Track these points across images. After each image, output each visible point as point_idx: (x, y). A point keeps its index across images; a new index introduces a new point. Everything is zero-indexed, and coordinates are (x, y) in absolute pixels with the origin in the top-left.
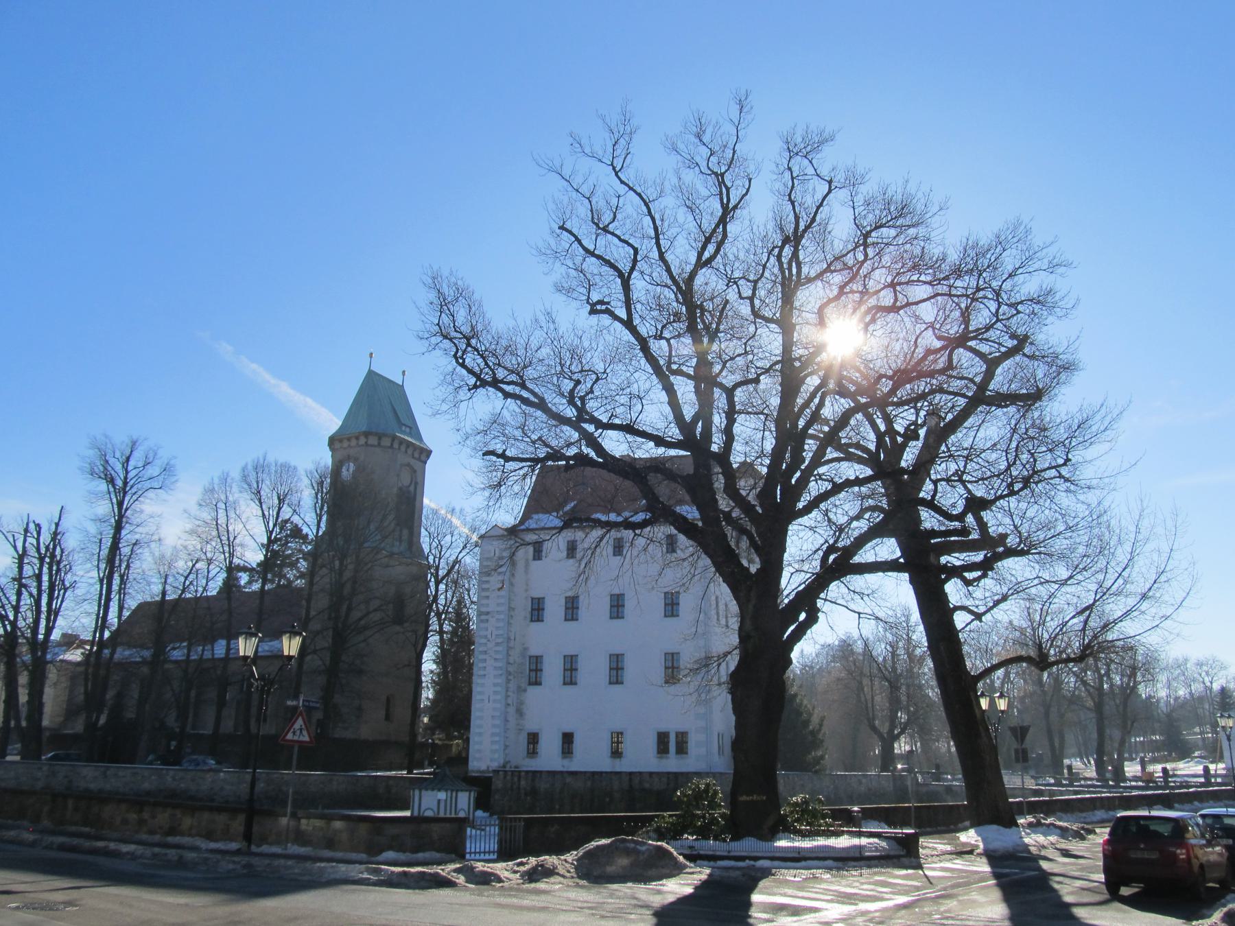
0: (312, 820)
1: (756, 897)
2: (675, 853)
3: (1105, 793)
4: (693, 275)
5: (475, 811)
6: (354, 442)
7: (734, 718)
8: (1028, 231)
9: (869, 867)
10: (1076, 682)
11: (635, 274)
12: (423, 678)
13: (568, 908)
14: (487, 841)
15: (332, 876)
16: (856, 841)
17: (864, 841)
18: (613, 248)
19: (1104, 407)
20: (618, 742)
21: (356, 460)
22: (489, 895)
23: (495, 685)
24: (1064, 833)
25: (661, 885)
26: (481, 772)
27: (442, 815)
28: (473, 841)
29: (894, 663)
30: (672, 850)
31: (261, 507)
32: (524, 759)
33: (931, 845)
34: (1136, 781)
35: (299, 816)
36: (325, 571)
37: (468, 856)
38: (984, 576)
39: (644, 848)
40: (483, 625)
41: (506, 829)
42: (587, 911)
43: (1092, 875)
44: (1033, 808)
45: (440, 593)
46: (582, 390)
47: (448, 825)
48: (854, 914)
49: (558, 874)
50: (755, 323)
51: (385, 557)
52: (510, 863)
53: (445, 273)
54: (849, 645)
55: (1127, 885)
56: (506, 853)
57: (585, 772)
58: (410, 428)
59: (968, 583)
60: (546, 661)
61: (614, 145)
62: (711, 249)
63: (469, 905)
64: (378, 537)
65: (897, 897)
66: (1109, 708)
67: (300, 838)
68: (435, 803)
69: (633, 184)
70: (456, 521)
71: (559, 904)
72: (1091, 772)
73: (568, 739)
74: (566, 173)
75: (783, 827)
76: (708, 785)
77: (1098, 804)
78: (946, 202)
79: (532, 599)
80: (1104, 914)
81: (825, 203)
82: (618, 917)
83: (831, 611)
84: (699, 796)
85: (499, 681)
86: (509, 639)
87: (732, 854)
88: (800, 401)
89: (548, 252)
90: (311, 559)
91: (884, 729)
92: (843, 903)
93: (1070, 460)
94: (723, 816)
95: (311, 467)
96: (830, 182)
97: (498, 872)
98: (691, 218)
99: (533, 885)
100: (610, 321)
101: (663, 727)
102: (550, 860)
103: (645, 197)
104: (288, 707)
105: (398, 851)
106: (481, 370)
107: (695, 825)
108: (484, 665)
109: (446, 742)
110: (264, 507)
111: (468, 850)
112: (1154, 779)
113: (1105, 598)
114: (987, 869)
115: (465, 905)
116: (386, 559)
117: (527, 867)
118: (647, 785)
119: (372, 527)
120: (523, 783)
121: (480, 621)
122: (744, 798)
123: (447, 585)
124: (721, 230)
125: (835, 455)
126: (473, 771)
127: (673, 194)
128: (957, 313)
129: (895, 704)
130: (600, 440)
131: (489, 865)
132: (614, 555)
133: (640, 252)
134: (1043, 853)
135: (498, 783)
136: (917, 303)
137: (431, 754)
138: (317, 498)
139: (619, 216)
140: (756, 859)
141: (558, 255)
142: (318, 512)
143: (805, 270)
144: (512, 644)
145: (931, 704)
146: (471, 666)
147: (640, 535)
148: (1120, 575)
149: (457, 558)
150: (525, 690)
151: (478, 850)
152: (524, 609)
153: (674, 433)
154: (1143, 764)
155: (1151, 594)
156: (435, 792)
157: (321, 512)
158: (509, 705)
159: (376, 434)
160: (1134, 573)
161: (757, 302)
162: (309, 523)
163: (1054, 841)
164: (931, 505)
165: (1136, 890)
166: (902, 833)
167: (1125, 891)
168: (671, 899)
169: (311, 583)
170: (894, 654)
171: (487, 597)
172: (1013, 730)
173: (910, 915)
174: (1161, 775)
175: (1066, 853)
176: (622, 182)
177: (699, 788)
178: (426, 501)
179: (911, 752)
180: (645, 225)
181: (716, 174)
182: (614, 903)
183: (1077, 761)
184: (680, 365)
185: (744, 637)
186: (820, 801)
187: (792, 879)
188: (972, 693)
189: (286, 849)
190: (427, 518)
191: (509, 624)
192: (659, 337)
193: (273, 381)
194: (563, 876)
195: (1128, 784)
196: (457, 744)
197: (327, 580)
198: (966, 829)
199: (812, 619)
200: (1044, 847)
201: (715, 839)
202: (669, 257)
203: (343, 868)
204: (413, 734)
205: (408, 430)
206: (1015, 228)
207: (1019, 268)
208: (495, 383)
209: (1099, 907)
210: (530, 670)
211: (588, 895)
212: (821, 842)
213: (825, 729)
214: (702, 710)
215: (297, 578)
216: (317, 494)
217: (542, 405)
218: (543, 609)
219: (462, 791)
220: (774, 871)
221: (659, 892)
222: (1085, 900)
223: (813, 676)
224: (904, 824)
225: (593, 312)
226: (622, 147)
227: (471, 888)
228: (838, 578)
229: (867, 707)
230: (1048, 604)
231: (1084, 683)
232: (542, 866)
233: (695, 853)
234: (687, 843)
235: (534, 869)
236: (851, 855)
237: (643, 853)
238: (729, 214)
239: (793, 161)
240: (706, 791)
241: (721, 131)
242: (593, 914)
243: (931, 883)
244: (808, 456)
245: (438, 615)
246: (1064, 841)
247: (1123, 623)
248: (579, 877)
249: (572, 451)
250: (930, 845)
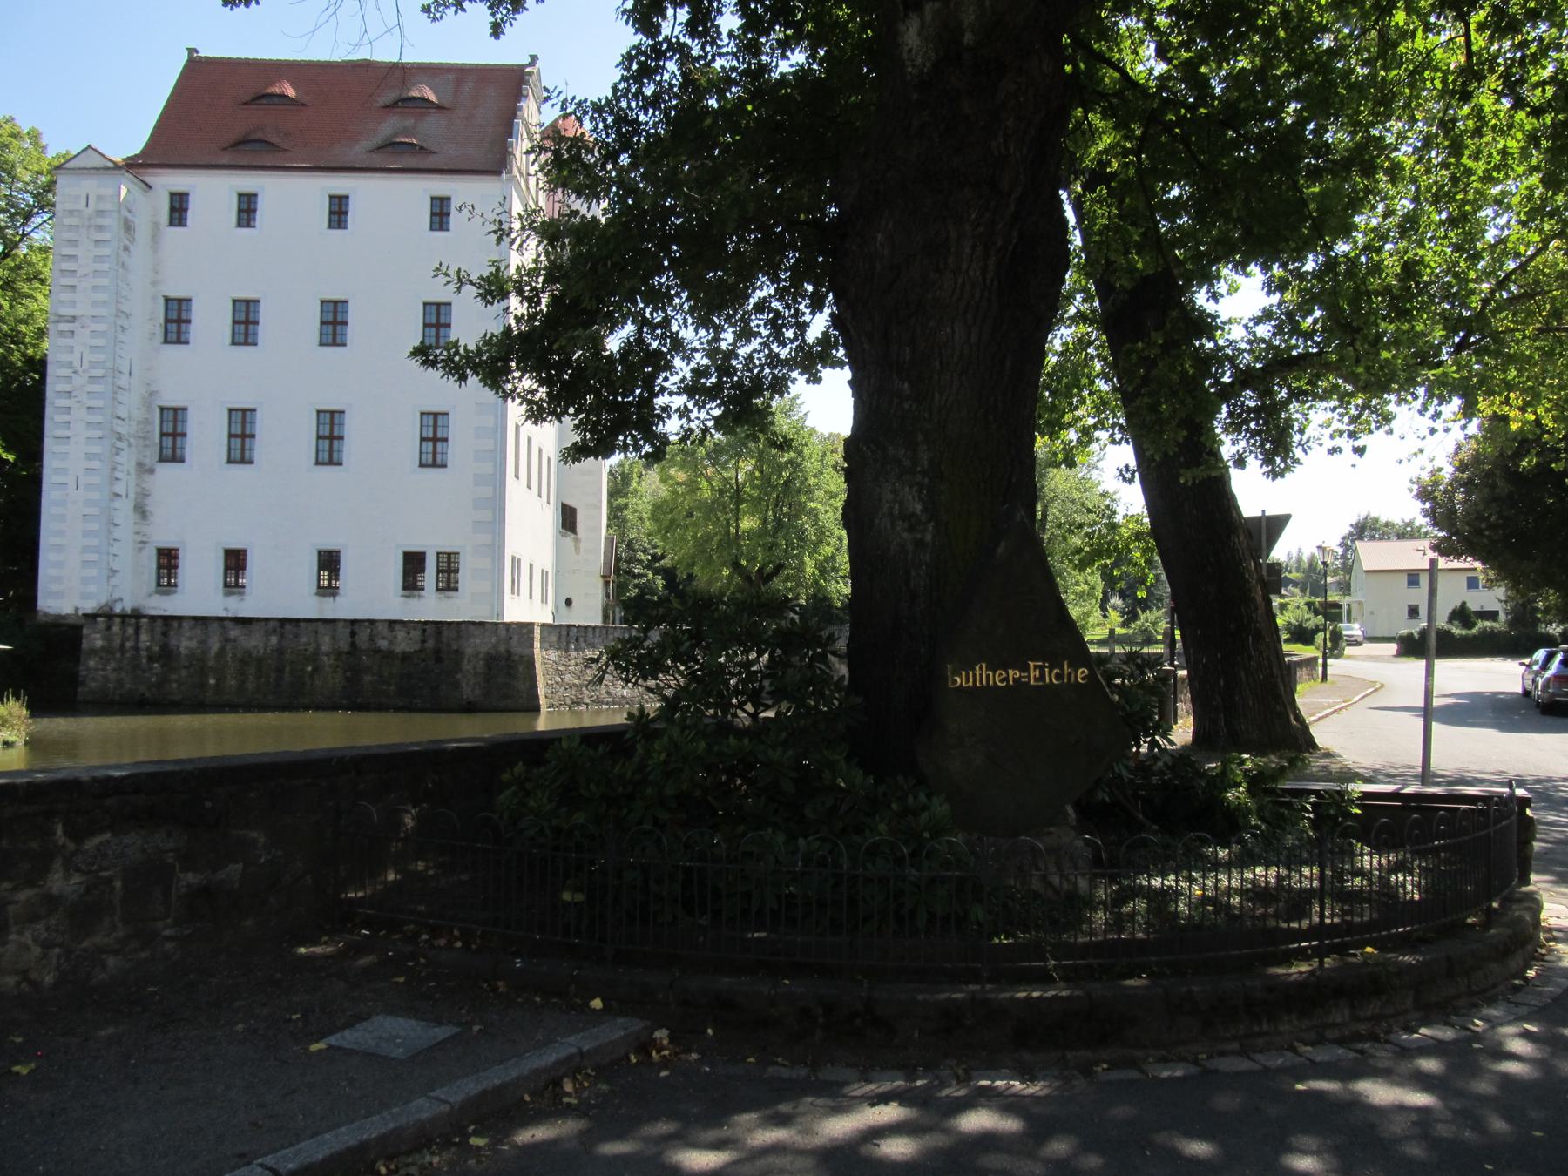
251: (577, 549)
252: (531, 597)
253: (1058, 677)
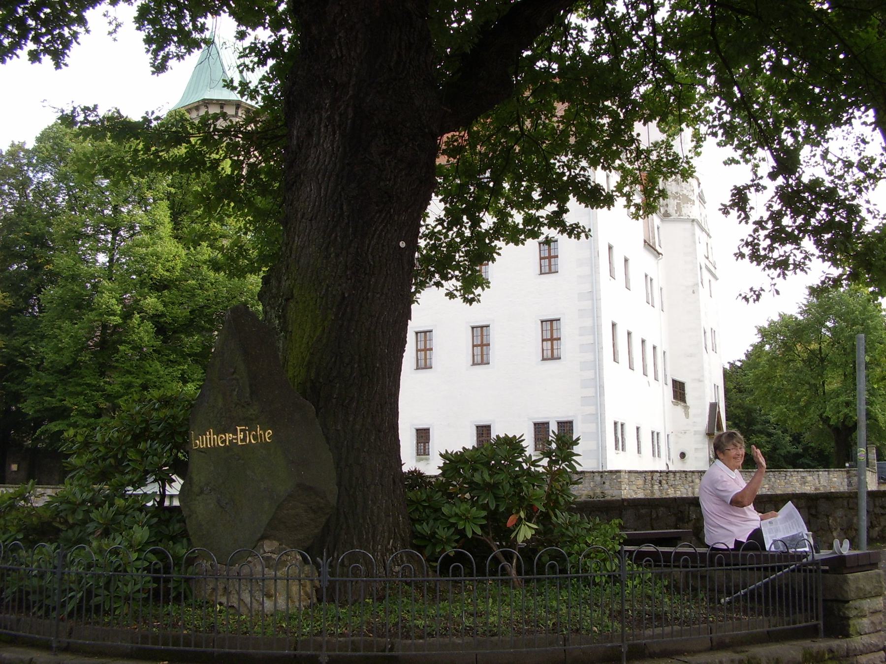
251: (687, 415)
252: (639, 451)
253: (255, 438)
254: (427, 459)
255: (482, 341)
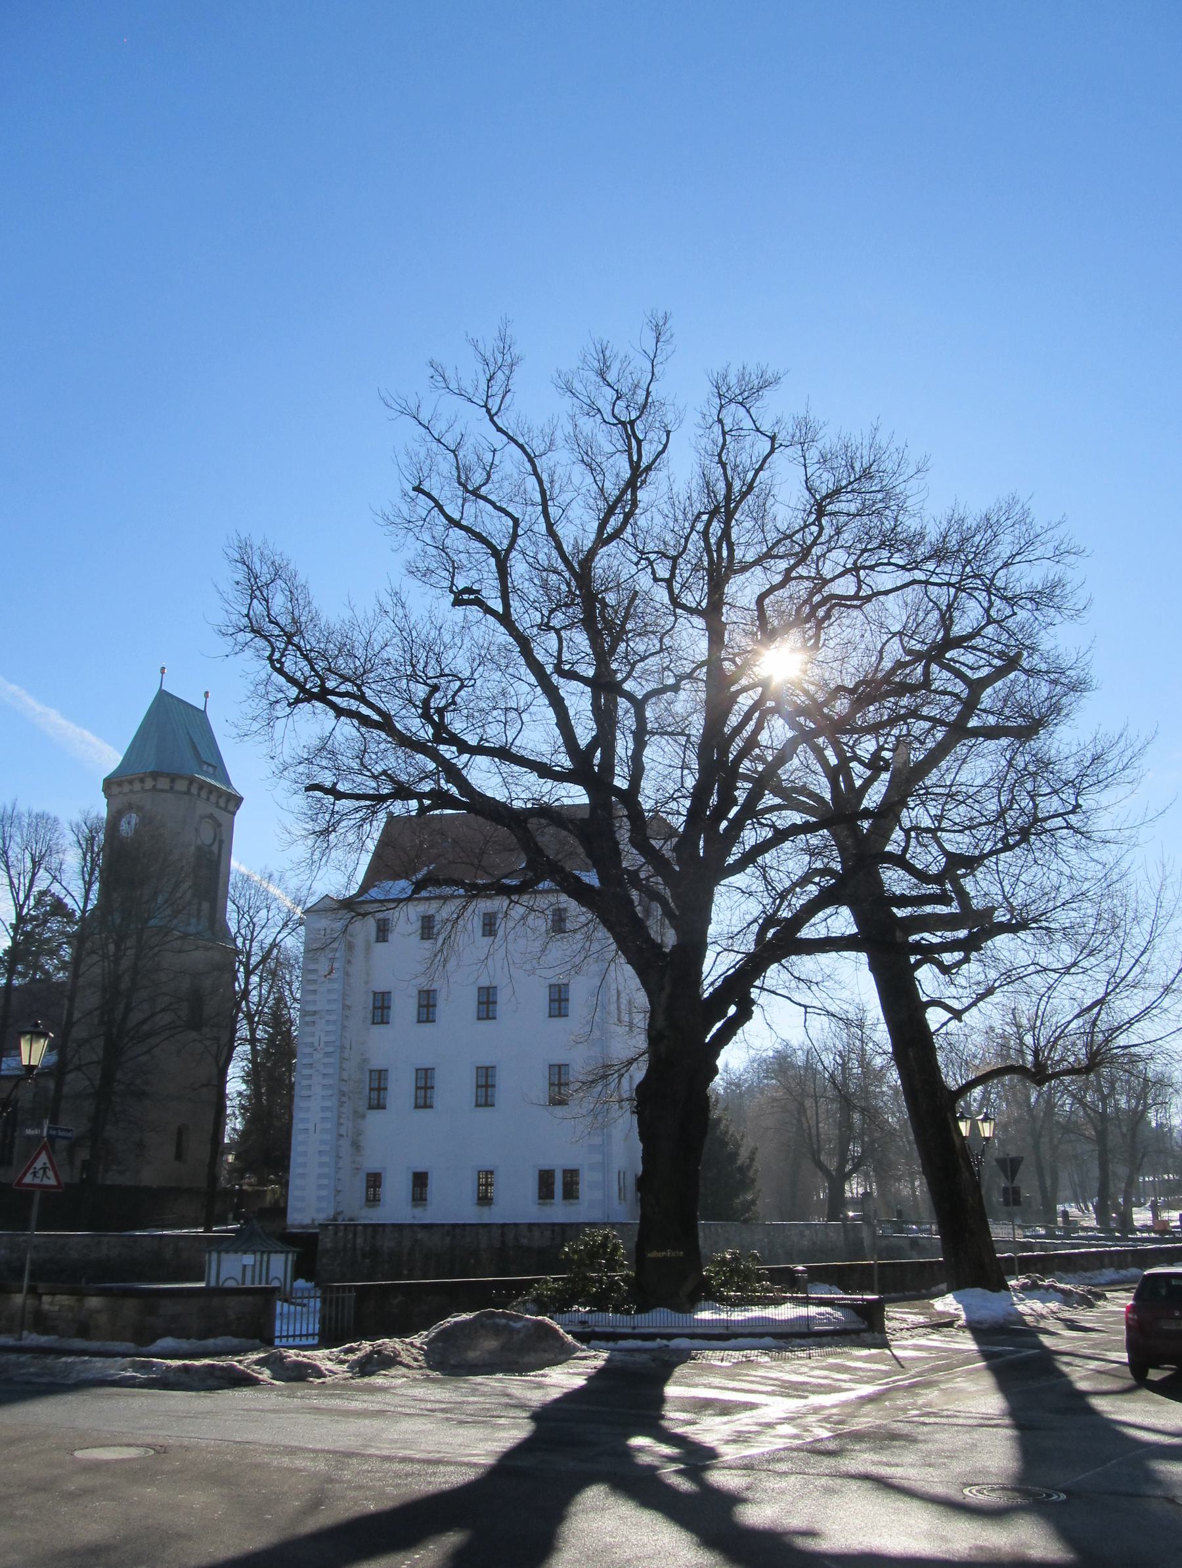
0: (58, 1298)
1: (671, 1390)
2: (561, 1331)
3: (1110, 1246)
4: (592, 553)
5: (295, 1278)
6: (137, 786)
7: (641, 1146)
8: (1026, 513)
9: (820, 1346)
10: (1072, 1105)
11: (513, 554)
12: (228, 1103)
13: (412, 1411)
14: (305, 1322)
15: (83, 1376)
16: (802, 1311)
17: (813, 1311)
18: (486, 519)
19: (1123, 739)
20: (487, 1185)
21: (140, 809)
22: (305, 1396)
23: (324, 1109)
24: (1067, 1298)
25: (542, 1376)
26: (303, 1227)
27: (248, 1285)
28: (285, 1321)
29: (845, 1078)
30: (557, 1327)
31: (8, 872)
32: (361, 1208)
33: (898, 1316)
34: (1149, 1232)
35: (41, 1291)
36: (96, 958)
37: (277, 1342)
38: (966, 960)
39: (519, 1325)
40: (307, 1029)
41: (331, 1303)
42: (440, 1415)
43: (1108, 1353)
44: (1025, 1265)
45: (251, 987)
46: (438, 701)
47: (250, 1298)
48: (804, 1410)
49: (401, 1363)
50: (675, 615)
51: (176, 939)
52: (335, 1350)
53: (257, 542)
54: (785, 1057)
55: (1156, 1366)
56: (329, 1337)
57: (443, 1225)
58: (215, 767)
59: (945, 970)
60: (392, 1076)
61: (489, 381)
62: (614, 522)
63: (274, 1411)
64: (168, 912)
65: (858, 1386)
66: (1114, 1138)
67: (41, 1322)
68: (240, 1269)
69: (513, 431)
70: (274, 890)
71: (400, 1406)
72: (1091, 1221)
73: (420, 1180)
74: (424, 417)
75: (707, 1294)
76: (606, 1237)
77: (1106, 1261)
78: (925, 463)
79: (375, 994)
80: (1132, 1406)
81: (766, 465)
82: (483, 1422)
83: (769, 1005)
84: (594, 1252)
85: (328, 1104)
86: (343, 1047)
87: (637, 1331)
88: (734, 720)
89: (398, 521)
90: (75, 942)
91: (832, 1165)
92: (789, 1396)
93: (1080, 806)
94: (626, 1279)
95: (77, 818)
96: (773, 439)
97: (318, 1363)
98: (590, 479)
99: (366, 1380)
100: (481, 615)
101: (546, 1163)
102: (391, 1344)
103: (529, 450)
104: (29, 1137)
105: (179, 1337)
106: (306, 679)
107: (589, 1292)
108: (309, 1082)
109: (256, 1188)
110: (13, 872)
111: (277, 1334)
112: (1169, 1229)
113: (1117, 990)
114: (972, 1346)
115: (268, 1411)
116: (179, 942)
117: (359, 1354)
118: (525, 1241)
119: (160, 900)
120: (359, 1241)
121: (304, 1024)
122: (654, 1254)
123: (261, 977)
124: (629, 497)
125: (778, 801)
126: (293, 1226)
127: (567, 446)
128: (935, 615)
129: (846, 1133)
130: (464, 772)
131: (306, 1353)
132: (484, 935)
133: (522, 524)
134: (1042, 1325)
135: (326, 1242)
136: (887, 593)
137: (238, 1205)
138: (85, 859)
139: (494, 477)
140: (670, 1337)
141: (411, 526)
142: (87, 878)
143: (738, 553)
144: (346, 1055)
145: (892, 1133)
146: (291, 1086)
147: (517, 903)
148: (1137, 961)
149: (275, 940)
150: (363, 1116)
151: (298, 1333)
152: (362, 1004)
153: (564, 761)
154: (1155, 1209)
155: (1174, 987)
156: (240, 1254)
157: (90, 879)
158: (341, 1136)
159: (168, 775)
160: (1154, 958)
161: (677, 587)
162: (74, 894)
163: (1055, 1309)
164: (900, 861)
165: (1167, 1373)
166: (863, 1300)
167: (1154, 1375)
168: (555, 1394)
169: (76, 975)
170: (844, 1065)
171: (315, 992)
172: (1001, 1162)
173: (880, 1411)
174: (1178, 1223)
175: (1072, 1325)
176: (499, 429)
177: (595, 1241)
178: (234, 863)
179: (865, 1194)
180: (529, 488)
181: (623, 423)
182: (477, 1403)
183: (1071, 1207)
184: (573, 664)
185: (655, 1036)
186: (754, 1257)
187: (719, 1363)
188: (949, 1114)
189: (20, 1339)
190: (236, 887)
191: (344, 1027)
192: (546, 627)
193: (39, 708)
194: (408, 1366)
195: (1139, 1235)
196: (273, 1190)
197: (97, 970)
198: (941, 1294)
199: (745, 1014)
200: (1042, 1317)
201: (616, 1310)
202: (560, 530)
203: (98, 1362)
204: (213, 1179)
205: (211, 770)
206: (1010, 507)
207: (1018, 554)
208: (323, 695)
209: (1120, 1397)
210: (371, 1089)
211: (440, 1393)
212: (756, 1312)
213: (757, 1165)
214: (597, 1140)
215: (58, 969)
216: (85, 855)
217: (386, 724)
218: (389, 1008)
219: (276, 1252)
220: (694, 1353)
221: (540, 1386)
222: (1105, 1387)
223: (741, 1095)
224: (863, 1289)
225: (458, 602)
226: (499, 382)
227: (279, 1386)
228: (778, 961)
229: (810, 1134)
230: (1045, 999)
231: (1084, 1105)
232: (379, 1352)
233: (588, 1330)
234: (577, 1317)
235: (369, 1357)
236: (797, 1329)
237: (518, 1331)
238: (640, 476)
239: (724, 411)
240: (604, 1245)
241: (631, 368)
242: (447, 1419)
243: (902, 1367)
244: (741, 795)
245: (249, 1017)
246: (1068, 1308)
247: (1141, 1023)
248: (431, 1368)
249: (426, 787)
250: (899, 1316)
254: (424, 1205)
255: (379, 1085)
